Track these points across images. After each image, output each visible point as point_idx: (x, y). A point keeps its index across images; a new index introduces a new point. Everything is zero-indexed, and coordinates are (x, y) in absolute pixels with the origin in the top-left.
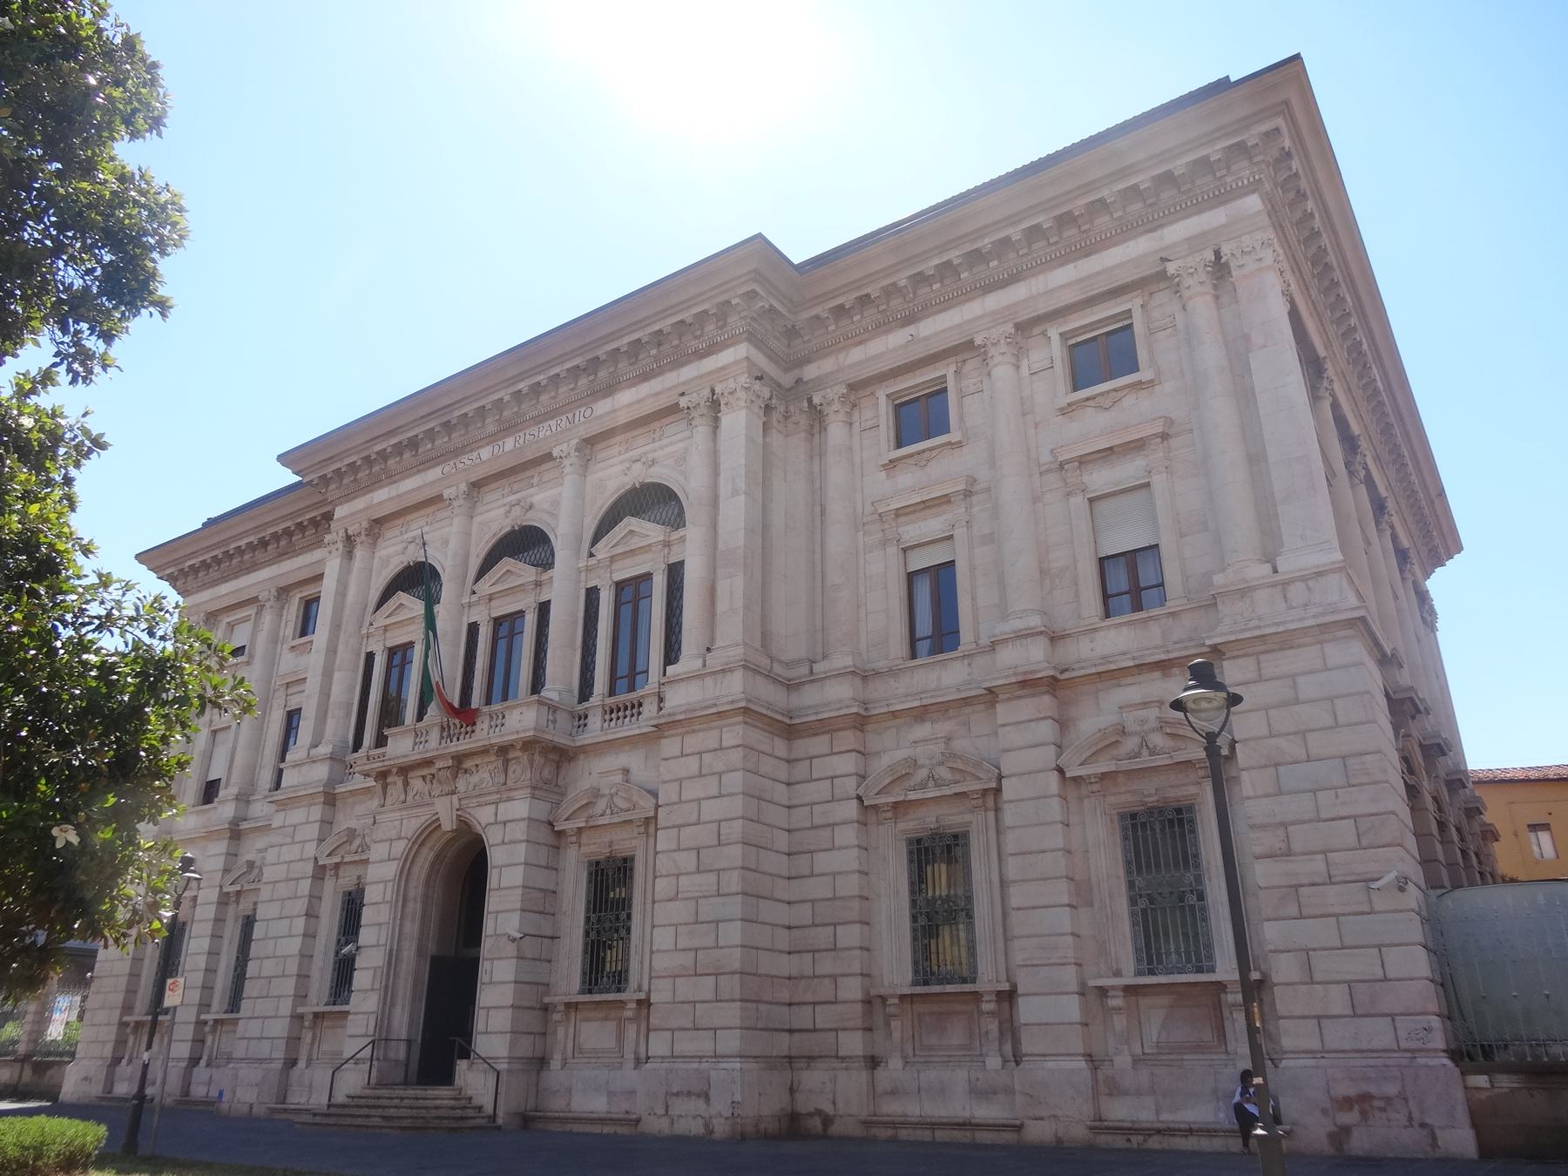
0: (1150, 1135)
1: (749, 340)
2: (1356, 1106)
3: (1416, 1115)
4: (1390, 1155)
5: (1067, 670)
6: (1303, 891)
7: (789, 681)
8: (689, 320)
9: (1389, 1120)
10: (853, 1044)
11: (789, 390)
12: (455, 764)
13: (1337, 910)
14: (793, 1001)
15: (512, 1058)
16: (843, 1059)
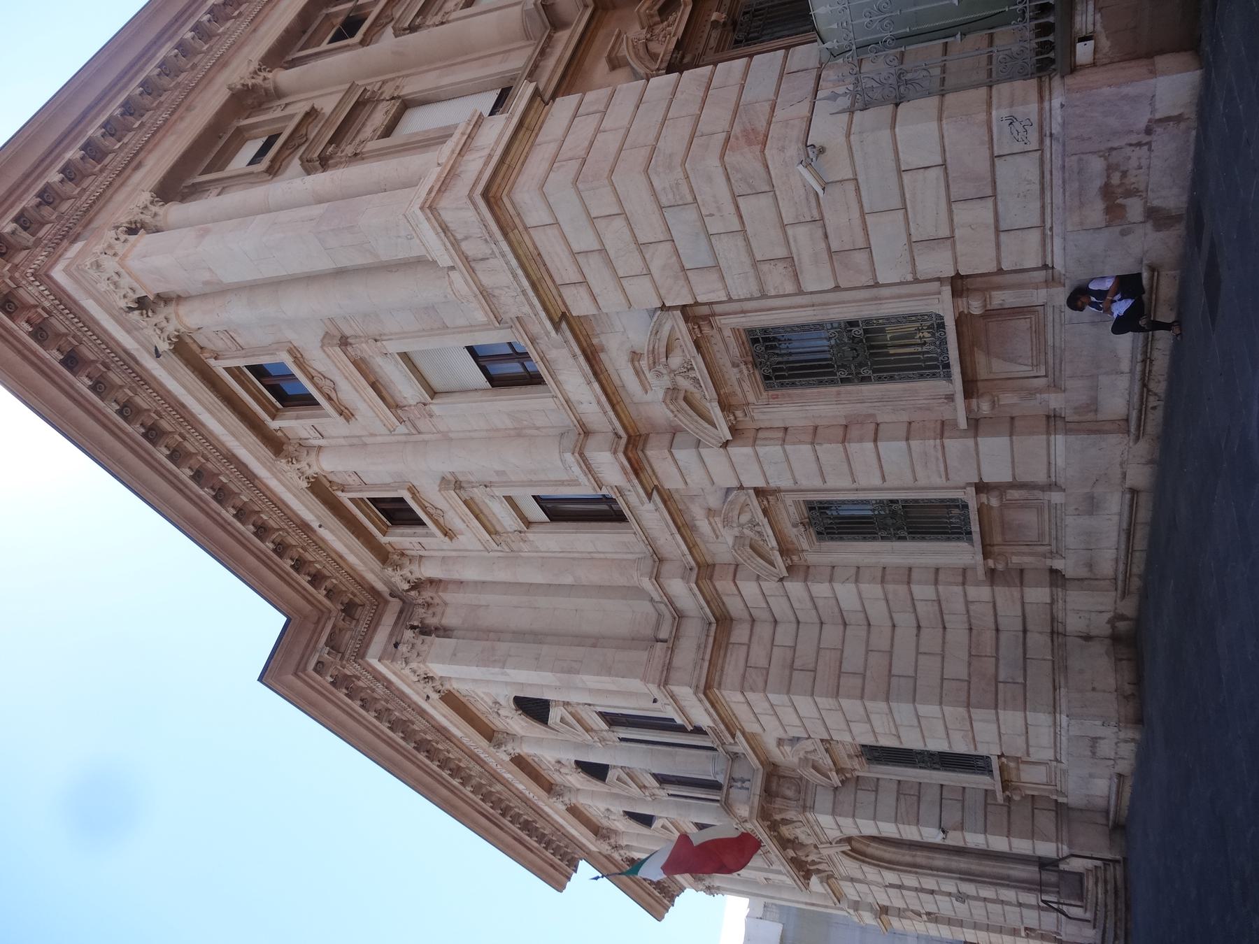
0: (1149, 391)
1: (363, 657)
2: (1118, 201)
3: (1134, 139)
4: (1190, 167)
5: (616, 434)
6: (834, 247)
7: (675, 618)
8: (359, 703)
9: (1140, 168)
10: (1038, 595)
11: (404, 602)
12: (789, 845)
13: (856, 214)
14: (994, 627)
15: (1057, 838)
16: (1053, 599)
